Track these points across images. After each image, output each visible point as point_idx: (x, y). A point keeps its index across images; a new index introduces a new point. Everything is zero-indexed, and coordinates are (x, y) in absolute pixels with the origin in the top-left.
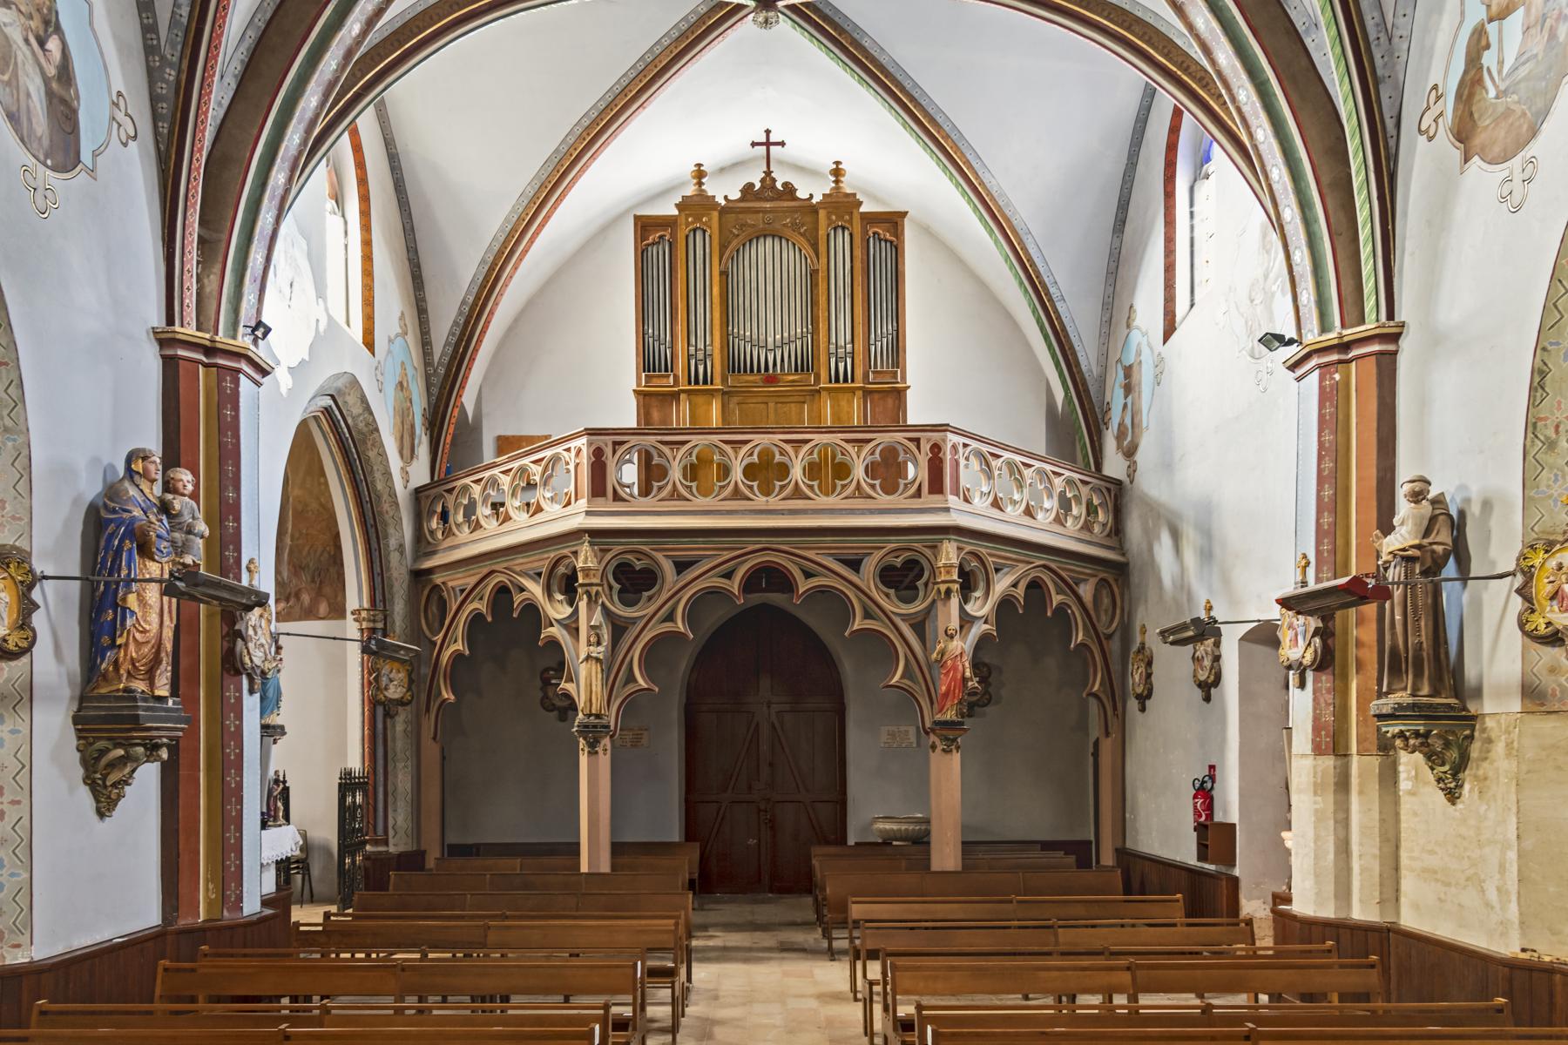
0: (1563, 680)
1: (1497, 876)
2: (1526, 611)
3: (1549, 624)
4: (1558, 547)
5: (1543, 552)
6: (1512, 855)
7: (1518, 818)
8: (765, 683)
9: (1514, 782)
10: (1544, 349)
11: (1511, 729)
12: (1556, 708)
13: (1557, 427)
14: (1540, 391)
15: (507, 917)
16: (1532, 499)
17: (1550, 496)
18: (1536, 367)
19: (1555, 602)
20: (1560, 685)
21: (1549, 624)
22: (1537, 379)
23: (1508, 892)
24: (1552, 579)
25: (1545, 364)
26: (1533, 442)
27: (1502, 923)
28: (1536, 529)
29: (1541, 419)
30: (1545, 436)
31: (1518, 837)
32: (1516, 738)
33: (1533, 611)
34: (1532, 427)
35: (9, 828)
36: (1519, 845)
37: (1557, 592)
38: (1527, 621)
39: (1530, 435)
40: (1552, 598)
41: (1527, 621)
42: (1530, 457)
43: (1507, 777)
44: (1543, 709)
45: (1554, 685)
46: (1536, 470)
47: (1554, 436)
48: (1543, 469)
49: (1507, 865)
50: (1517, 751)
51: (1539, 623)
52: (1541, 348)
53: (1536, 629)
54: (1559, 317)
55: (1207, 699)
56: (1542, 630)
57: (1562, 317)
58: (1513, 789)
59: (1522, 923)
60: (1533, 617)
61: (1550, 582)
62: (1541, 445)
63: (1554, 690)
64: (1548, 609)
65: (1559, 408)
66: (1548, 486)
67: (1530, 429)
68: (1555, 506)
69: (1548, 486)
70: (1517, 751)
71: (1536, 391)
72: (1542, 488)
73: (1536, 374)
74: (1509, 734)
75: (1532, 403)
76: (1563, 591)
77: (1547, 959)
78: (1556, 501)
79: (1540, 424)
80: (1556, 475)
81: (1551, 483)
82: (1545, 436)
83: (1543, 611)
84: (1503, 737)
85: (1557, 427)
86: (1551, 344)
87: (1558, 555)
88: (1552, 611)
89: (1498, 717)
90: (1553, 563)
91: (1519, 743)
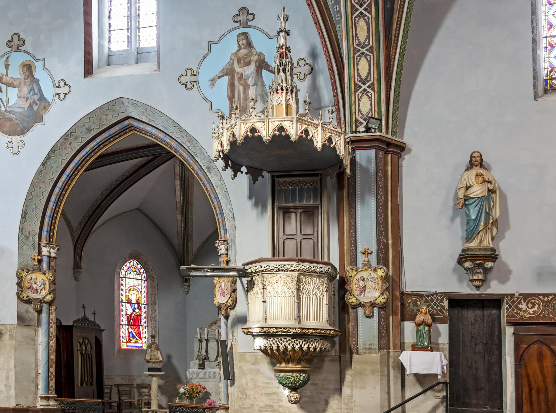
0: (30, 315)
1: (5, 381)
2: (20, 291)
3: (27, 296)
4: (31, 272)
5: (26, 272)
6: (12, 373)
7: (15, 361)
8: (346, 287)
9: (14, 348)
10: (26, 206)
11: (12, 330)
12: (27, 324)
13: (29, 232)
14: (24, 219)
15: (538, 395)
16: (21, 254)
17: (27, 254)
18: (24, 211)
19: (29, 290)
20: (29, 317)
21: (27, 296)
22: (24, 215)
23: (10, 386)
24: (29, 282)
25: (26, 211)
26: (21, 235)
27: (7, 397)
28: (22, 264)
29: (24, 228)
30: (25, 234)
31: (15, 367)
32: (14, 333)
33: (22, 291)
34: (21, 230)
35: (34, 198)
36: (15, 370)
37: (31, 287)
38: (20, 295)
39: (20, 232)
40: (29, 288)
41: (20, 295)
42: (20, 240)
43: (10, 346)
44: (24, 324)
45: (27, 317)
46: (22, 245)
47: (28, 235)
48: (24, 245)
49: (10, 377)
50: (15, 338)
51: (24, 296)
52: (26, 205)
53: (23, 297)
54: (32, 197)
55: (94, 311)
56: (25, 298)
57: (33, 198)
58: (13, 350)
59: (16, 396)
60: (23, 293)
61: (28, 283)
62: (24, 237)
63: (27, 318)
64: (27, 291)
65: (30, 227)
66: (26, 251)
67: (20, 231)
68: (28, 258)
69: (26, 251)
70: (15, 338)
71: (23, 218)
72: (24, 251)
73: (23, 213)
74: (11, 331)
75: (21, 222)
76: (33, 286)
77: (25, 407)
78: (28, 256)
79: (24, 230)
80: (28, 248)
81: (27, 250)
82: (25, 234)
83: (26, 292)
84: (8, 333)
85: (29, 232)
86: (29, 205)
87: (31, 274)
88: (28, 292)
89: (6, 326)
90: (29, 277)
91: (15, 335)
